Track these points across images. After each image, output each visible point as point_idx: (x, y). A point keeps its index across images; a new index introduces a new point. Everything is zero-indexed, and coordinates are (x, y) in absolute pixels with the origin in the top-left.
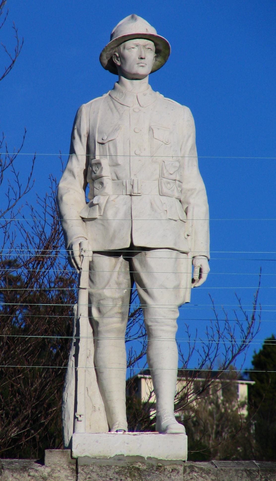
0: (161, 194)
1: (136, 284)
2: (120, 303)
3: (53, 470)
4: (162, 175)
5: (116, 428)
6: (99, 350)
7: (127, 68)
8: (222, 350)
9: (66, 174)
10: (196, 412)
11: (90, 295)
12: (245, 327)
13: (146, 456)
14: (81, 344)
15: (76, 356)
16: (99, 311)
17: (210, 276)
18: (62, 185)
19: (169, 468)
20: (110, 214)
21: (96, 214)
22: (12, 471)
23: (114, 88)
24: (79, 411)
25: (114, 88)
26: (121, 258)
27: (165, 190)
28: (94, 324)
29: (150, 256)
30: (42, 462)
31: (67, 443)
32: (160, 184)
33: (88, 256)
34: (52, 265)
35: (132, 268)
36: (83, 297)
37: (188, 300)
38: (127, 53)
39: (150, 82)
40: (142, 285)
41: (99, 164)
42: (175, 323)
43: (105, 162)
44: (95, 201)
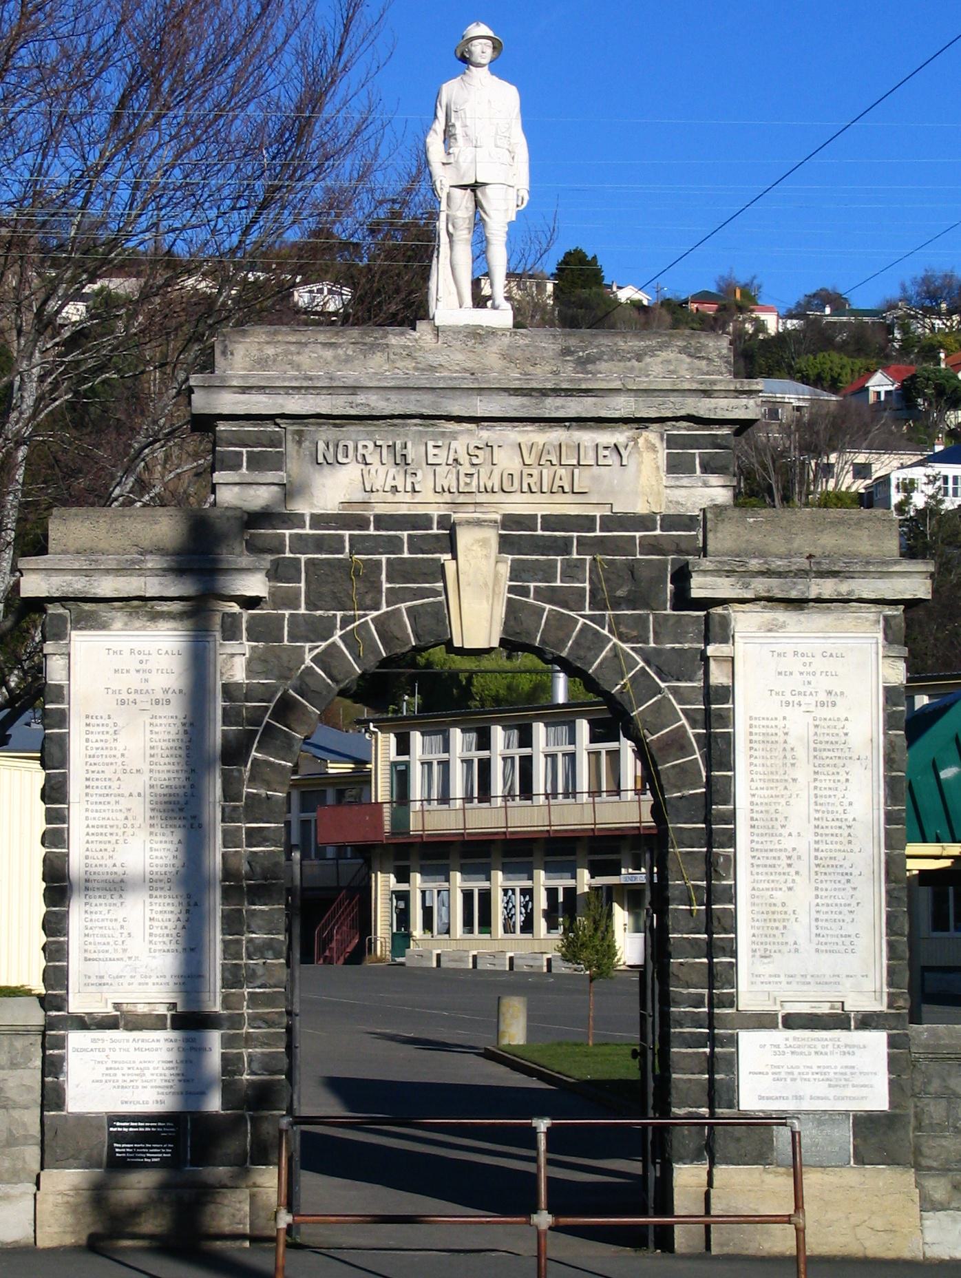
0: (497, 146)
1: (479, 209)
2: (467, 221)
3: (422, 335)
4: (497, 134)
5: (464, 306)
6: (454, 253)
7: (473, 59)
8: (533, 251)
9: (431, 132)
10: (519, 301)
11: (448, 216)
12: (548, 236)
13: (484, 325)
14: (441, 249)
15: (438, 257)
16: (454, 227)
17: (529, 202)
18: (428, 140)
19: (500, 333)
20: (461, 160)
21: (452, 160)
22: (395, 335)
23: (465, 73)
24: (440, 295)
25: (465, 73)
26: (469, 191)
27: (499, 144)
28: (450, 235)
29: (488, 189)
30: (414, 329)
31: (431, 317)
32: (495, 139)
33: (446, 190)
34: (416, 194)
35: (476, 196)
36: (443, 217)
37: (514, 219)
38: (473, 48)
39: (490, 69)
40: (482, 208)
41: (453, 126)
42: (505, 235)
43: (458, 125)
44: (451, 151)
